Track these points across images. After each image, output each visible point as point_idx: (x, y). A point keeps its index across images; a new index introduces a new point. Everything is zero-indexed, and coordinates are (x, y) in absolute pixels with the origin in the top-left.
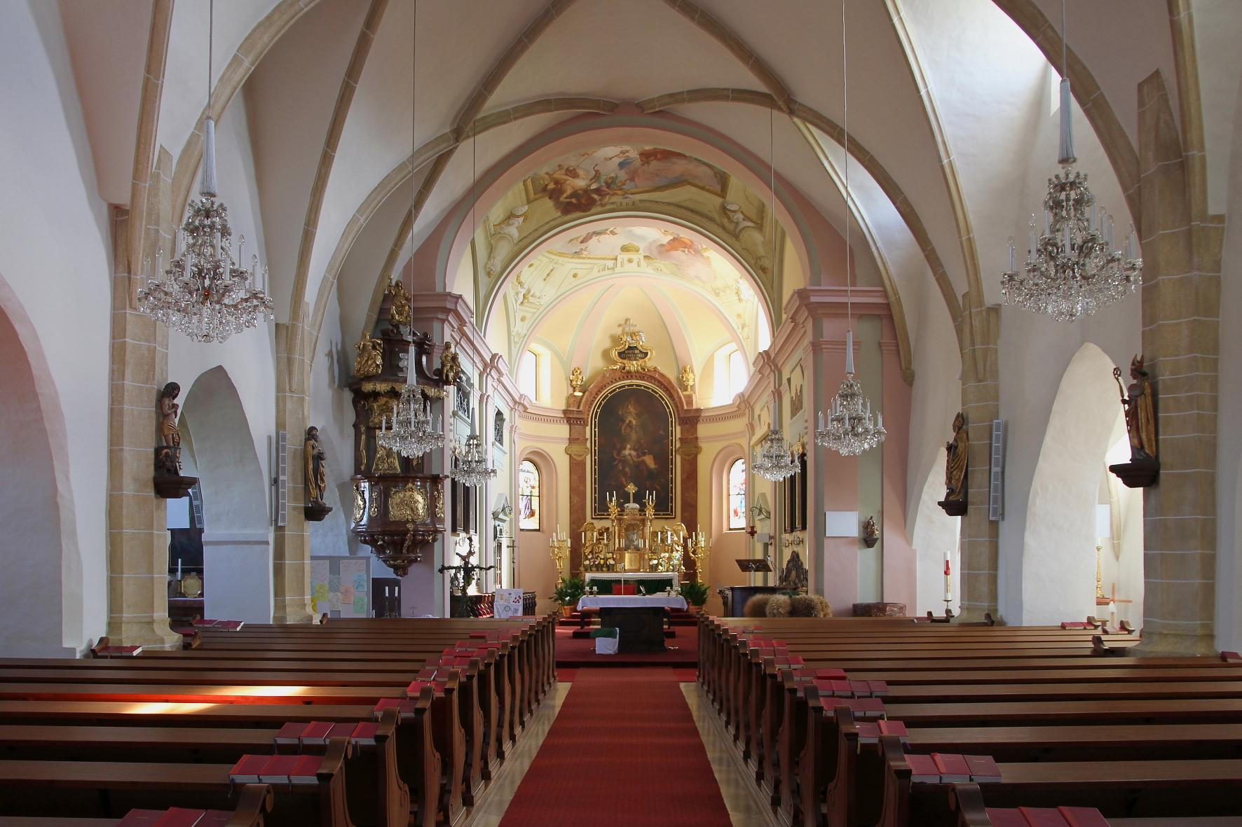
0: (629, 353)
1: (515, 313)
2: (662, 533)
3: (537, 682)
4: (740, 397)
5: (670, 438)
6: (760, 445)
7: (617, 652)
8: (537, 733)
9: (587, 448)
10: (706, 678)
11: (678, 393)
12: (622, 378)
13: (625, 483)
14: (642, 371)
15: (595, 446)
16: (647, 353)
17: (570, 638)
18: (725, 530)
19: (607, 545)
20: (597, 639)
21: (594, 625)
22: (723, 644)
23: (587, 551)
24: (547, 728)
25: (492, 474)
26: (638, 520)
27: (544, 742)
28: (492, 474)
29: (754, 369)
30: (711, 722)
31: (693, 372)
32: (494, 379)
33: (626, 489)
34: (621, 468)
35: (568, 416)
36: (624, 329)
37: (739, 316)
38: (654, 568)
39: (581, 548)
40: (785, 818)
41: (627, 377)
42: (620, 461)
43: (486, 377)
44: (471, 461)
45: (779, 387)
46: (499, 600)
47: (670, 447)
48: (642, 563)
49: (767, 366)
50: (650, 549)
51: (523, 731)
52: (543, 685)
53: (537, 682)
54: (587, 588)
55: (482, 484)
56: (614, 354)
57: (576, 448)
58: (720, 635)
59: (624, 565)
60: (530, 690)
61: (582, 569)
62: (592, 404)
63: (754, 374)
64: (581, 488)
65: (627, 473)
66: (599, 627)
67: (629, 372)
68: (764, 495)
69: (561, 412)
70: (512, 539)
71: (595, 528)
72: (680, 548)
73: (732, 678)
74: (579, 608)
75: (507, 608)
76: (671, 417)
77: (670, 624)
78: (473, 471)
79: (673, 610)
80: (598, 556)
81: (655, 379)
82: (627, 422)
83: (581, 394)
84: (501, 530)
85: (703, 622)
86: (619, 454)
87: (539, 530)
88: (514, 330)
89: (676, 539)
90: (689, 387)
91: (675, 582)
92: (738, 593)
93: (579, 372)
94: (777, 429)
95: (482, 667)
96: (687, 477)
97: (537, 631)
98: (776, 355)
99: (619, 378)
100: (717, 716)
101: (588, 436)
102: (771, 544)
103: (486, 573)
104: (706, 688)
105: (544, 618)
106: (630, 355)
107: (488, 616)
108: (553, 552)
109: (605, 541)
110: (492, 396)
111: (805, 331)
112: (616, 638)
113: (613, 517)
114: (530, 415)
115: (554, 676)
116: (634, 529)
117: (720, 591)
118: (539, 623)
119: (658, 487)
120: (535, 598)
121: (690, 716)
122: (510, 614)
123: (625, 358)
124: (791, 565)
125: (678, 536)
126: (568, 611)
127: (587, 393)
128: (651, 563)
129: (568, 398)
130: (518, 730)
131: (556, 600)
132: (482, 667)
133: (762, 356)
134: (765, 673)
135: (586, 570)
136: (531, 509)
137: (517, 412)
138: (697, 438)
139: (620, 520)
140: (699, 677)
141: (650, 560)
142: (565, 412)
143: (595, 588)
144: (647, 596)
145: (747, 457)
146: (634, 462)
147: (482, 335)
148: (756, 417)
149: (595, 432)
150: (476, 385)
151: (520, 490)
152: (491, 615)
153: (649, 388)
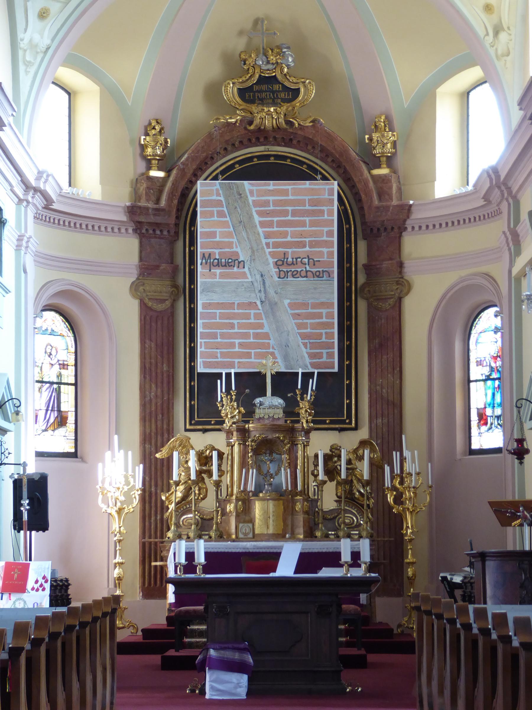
0: (261, 91)
4: (489, 176)
12: (245, 142)
16: (298, 90)
29: (522, 113)
35: (138, 219)
37: (488, 8)
48: (289, 522)
83: (161, 174)
87: (74, 455)
93: (158, 128)
99: (241, 142)
106: (264, 95)
113: (227, 424)
114: (57, 216)
127: (174, 172)
129: (135, 184)
136: (59, 411)
137: (31, 208)
139: (244, 433)
145: (505, 301)
147: (24, 141)
153: (302, 163)
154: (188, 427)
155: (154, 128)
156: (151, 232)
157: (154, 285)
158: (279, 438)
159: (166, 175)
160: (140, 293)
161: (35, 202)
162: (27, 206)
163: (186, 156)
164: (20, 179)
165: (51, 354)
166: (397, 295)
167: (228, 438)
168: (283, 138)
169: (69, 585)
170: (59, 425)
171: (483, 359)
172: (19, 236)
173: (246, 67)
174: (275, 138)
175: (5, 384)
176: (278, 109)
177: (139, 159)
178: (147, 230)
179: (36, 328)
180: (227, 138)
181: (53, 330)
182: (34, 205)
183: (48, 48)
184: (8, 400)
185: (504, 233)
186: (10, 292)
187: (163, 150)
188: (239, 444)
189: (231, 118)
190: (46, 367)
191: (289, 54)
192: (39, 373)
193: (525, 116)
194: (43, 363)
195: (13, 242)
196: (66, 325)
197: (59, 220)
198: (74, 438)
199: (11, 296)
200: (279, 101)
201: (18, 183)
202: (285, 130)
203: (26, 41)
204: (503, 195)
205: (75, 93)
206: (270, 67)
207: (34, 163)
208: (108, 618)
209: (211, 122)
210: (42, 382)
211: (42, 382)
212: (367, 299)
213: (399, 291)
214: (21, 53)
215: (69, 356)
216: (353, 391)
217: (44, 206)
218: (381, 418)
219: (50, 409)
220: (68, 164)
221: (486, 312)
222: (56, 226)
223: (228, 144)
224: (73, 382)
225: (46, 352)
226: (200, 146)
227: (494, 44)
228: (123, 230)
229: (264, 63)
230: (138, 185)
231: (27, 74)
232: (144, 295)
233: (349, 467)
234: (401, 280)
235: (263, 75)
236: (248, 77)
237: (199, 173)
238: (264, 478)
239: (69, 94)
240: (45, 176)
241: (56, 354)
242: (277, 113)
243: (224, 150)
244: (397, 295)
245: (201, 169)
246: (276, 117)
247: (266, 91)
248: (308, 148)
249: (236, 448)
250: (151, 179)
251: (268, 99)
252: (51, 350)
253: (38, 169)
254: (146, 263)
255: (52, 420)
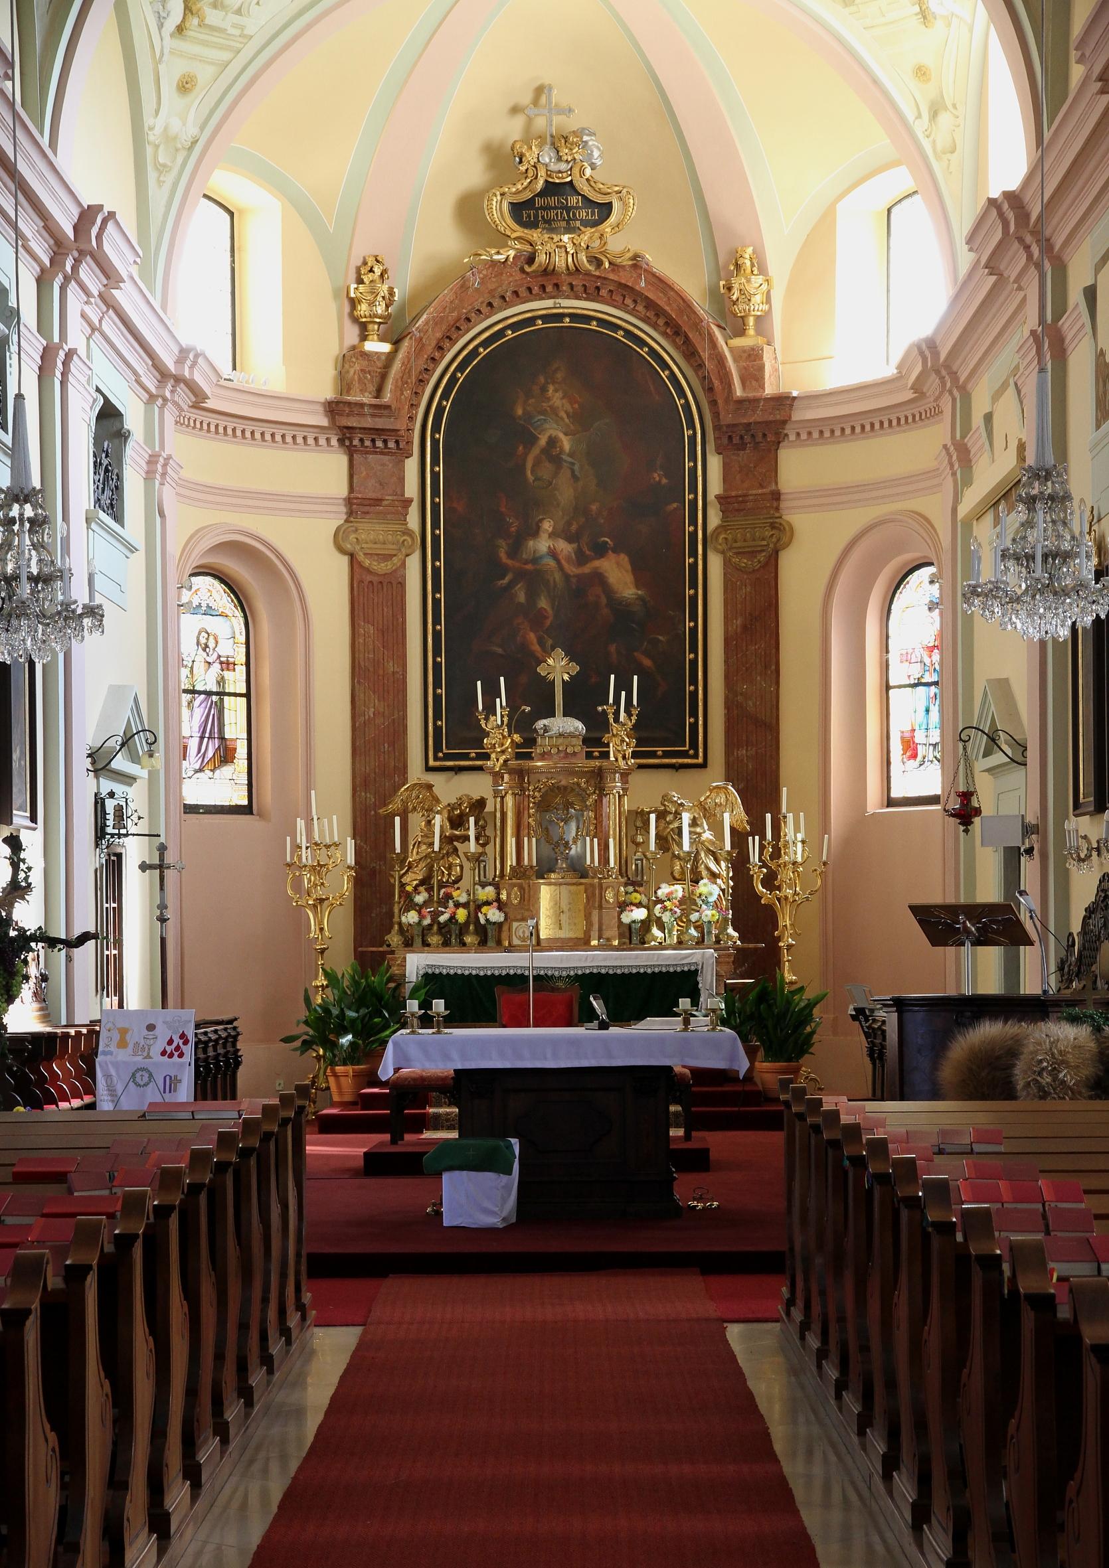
0: (547, 208)
1: (157, 62)
2: (661, 816)
3: (244, 1327)
4: (921, 353)
5: (688, 497)
6: (989, 517)
7: (514, 1220)
8: (244, 1506)
9: (409, 533)
10: (816, 1309)
11: (713, 344)
12: (523, 292)
13: (536, 647)
14: (591, 268)
15: (436, 525)
16: (610, 205)
17: (355, 1173)
18: (873, 801)
19: (477, 859)
20: (446, 1177)
21: (436, 1128)
22: (870, 1192)
23: (412, 879)
24: (277, 1490)
25: (87, 622)
26: (581, 774)
27: (267, 1538)
28: (87, 622)
30: (833, 1458)
31: (763, 271)
32: (88, 293)
33: (542, 670)
34: (522, 597)
36: (530, 121)
37: (921, 72)
38: (635, 936)
39: (392, 868)
40: (939, 1543)
41: (543, 287)
42: (520, 575)
43: (63, 289)
44: (16, 577)
45: (963, 437)
46: (113, 1048)
47: (689, 529)
49: (1016, 245)
50: (623, 870)
51: (194, 1497)
52: (264, 1338)
53: (244, 1327)
54: (413, 1006)
55: (55, 655)
56: (498, 211)
57: (372, 532)
58: (858, 1162)
59: (537, 927)
60: (219, 1357)
61: (394, 939)
62: (422, 382)
63: (970, 275)
64: (391, 667)
65: (541, 615)
66: (454, 1135)
67: (548, 272)
68: (1002, 686)
69: (320, 409)
70: (157, 841)
71: (438, 801)
72: (723, 868)
73: (902, 1312)
74: (386, 1071)
75: (139, 1076)
76: (691, 425)
77: (692, 1123)
78: (21, 611)
79: (700, 1074)
80: (449, 896)
81: (637, 296)
82: (543, 441)
83: (385, 348)
84: (119, 810)
85: (801, 1117)
86: (514, 552)
87: (247, 810)
88: (155, 125)
89: (707, 835)
90: (751, 321)
91: (707, 982)
92: (917, 1017)
93: (378, 270)
94: (1050, 460)
95: (54, 1281)
96: (745, 628)
97: (245, 1153)
98: (1049, 206)
99: (516, 293)
100: (855, 1439)
101: (411, 489)
102: (1029, 851)
103: (69, 959)
104: (814, 1342)
105: (266, 1109)
106: (552, 213)
107: (76, 1103)
108: (297, 882)
109: (472, 846)
110: (82, 352)
111: (1024, 299)
112: (509, 1172)
114: (214, 420)
115: (300, 1307)
116: (568, 805)
117: (860, 1011)
118: (249, 1126)
119: (647, 662)
120: (235, 1038)
121: (765, 1437)
122: (152, 1095)
123: (531, 225)
124: (1097, 921)
125: (717, 828)
126: (347, 1083)
127: (406, 344)
128: (626, 918)
130: (177, 1495)
131: (307, 1045)
132: (54, 1281)
133: (1001, 215)
134: (1014, 1291)
135: (408, 944)
136: (222, 738)
138: (777, 496)
139: (520, 774)
140: (790, 1303)
141: (623, 906)
142: (333, 408)
143: (439, 1005)
144: (614, 1030)
145: (946, 558)
146: (567, 577)
147: (45, 141)
148: (977, 420)
149: (435, 476)
150: (29, 315)
151: (185, 672)
152: (88, 1099)
153: (616, 327)
154: (432, 763)
155: (371, 271)
156: (368, 443)
157: (373, 530)
158: (578, 784)
159: (392, 348)
160: (352, 545)
161: (176, 399)
162: (162, 408)
163: (425, 316)
164: (150, 363)
165: (207, 646)
166: (771, 546)
167: (496, 784)
168: (584, 286)
169: (238, 1034)
170: (221, 761)
171: (910, 651)
172: (150, 456)
173: (523, 168)
174: (572, 286)
175: (132, 702)
176: (576, 237)
177: (347, 322)
178: (361, 440)
179: (182, 606)
180: (491, 286)
181: (208, 606)
182: (176, 404)
183: (195, 142)
184: (138, 732)
185: (945, 446)
186: (137, 550)
187: (387, 307)
188: (513, 793)
189: (498, 253)
190: (199, 668)
191: (594, 145)
192: (187, 677)
193: (978, 261)
194: (193, 661)
195: (141, 467)
196: (231, 598)
197: (217, 426)
198: (246, 782)
199: (139, 558)
200: (578, 224)
201: (148, 369)
202: (588, 274)
203: (158, 130)
204: (943, 384)
205: (241, 211)
206: (563, 166)
207: (174, 337)
208: (290, 1127)
209: (466, 260)
210: (193, 692)
211: (193, 692)
212: (723, 552)
213: (774, 540)
214: (149, 150)
215: (236, 649)
216: (700, 704)
217: (191, 404)
218: (745, 747)
219: (207, 735)
220: (230, 331)
221: (916, 573)
222: (212, 435)
223: (494, 297)
224: (244, 691)
225: (198, 643)
226: (447, 299)
227: (931, 133)
228: (322, 441)
229: (553, 160)
230: (347, 366)
231: (160, 186)
232: (358, 548)
233: (692, 829)
234: (777, 520)
235: (550, 180)
236: (525, 184)
237: (447, 344)
238: (554, 849)
239: (231, 214)
240: (191, 356)
241: (214, 645)
242: (574, 244)
243: (487, 306)
244: (771, 546)
245: (449, 338)
246: (572, 252)
247: (555, 208)
248: (625, 302)
249: (509, 801)
250: (366, 355)
251: (559, 221)
252: (207, 639)
253: (181, 346)
254: (360, 496)
255: (210, 754)
